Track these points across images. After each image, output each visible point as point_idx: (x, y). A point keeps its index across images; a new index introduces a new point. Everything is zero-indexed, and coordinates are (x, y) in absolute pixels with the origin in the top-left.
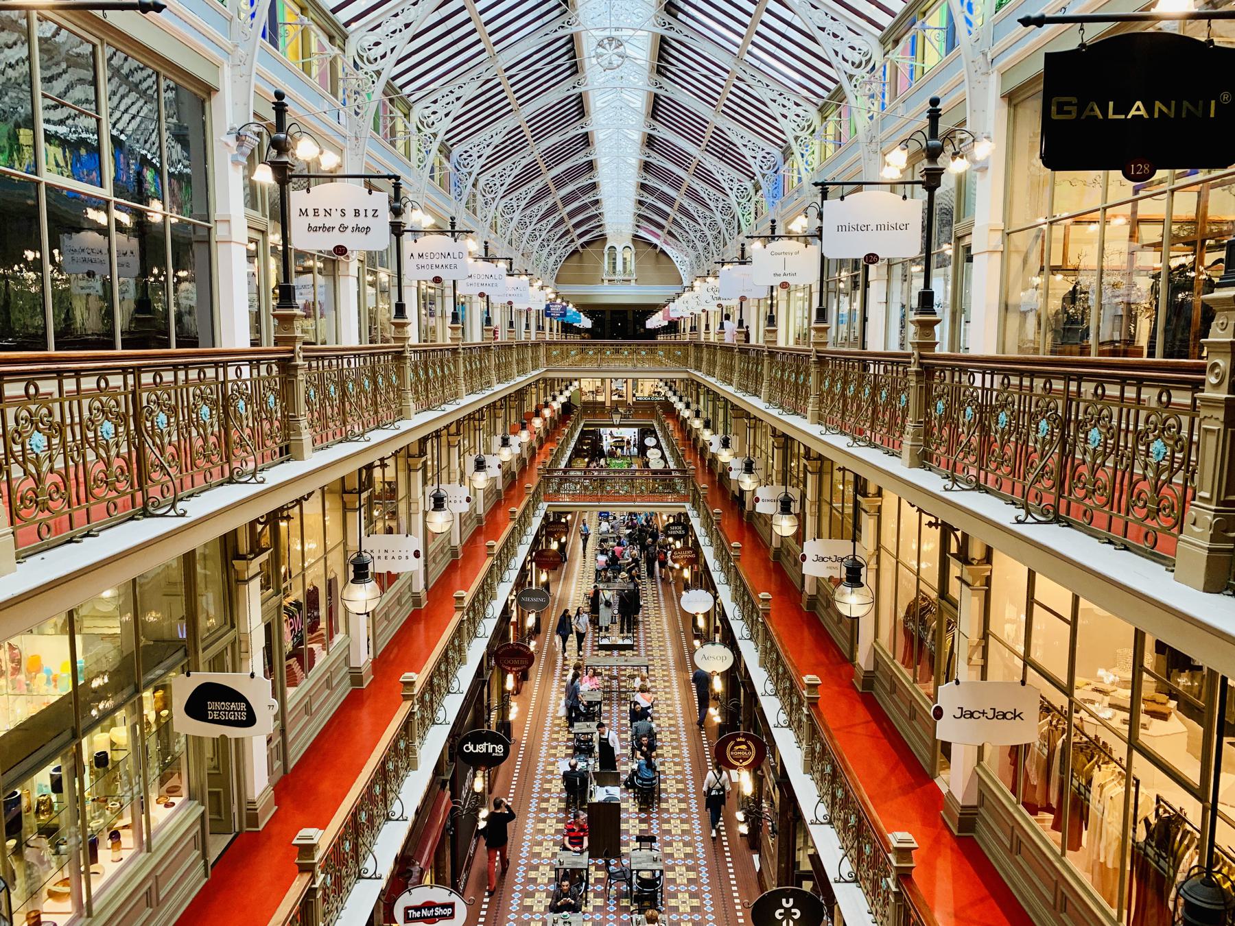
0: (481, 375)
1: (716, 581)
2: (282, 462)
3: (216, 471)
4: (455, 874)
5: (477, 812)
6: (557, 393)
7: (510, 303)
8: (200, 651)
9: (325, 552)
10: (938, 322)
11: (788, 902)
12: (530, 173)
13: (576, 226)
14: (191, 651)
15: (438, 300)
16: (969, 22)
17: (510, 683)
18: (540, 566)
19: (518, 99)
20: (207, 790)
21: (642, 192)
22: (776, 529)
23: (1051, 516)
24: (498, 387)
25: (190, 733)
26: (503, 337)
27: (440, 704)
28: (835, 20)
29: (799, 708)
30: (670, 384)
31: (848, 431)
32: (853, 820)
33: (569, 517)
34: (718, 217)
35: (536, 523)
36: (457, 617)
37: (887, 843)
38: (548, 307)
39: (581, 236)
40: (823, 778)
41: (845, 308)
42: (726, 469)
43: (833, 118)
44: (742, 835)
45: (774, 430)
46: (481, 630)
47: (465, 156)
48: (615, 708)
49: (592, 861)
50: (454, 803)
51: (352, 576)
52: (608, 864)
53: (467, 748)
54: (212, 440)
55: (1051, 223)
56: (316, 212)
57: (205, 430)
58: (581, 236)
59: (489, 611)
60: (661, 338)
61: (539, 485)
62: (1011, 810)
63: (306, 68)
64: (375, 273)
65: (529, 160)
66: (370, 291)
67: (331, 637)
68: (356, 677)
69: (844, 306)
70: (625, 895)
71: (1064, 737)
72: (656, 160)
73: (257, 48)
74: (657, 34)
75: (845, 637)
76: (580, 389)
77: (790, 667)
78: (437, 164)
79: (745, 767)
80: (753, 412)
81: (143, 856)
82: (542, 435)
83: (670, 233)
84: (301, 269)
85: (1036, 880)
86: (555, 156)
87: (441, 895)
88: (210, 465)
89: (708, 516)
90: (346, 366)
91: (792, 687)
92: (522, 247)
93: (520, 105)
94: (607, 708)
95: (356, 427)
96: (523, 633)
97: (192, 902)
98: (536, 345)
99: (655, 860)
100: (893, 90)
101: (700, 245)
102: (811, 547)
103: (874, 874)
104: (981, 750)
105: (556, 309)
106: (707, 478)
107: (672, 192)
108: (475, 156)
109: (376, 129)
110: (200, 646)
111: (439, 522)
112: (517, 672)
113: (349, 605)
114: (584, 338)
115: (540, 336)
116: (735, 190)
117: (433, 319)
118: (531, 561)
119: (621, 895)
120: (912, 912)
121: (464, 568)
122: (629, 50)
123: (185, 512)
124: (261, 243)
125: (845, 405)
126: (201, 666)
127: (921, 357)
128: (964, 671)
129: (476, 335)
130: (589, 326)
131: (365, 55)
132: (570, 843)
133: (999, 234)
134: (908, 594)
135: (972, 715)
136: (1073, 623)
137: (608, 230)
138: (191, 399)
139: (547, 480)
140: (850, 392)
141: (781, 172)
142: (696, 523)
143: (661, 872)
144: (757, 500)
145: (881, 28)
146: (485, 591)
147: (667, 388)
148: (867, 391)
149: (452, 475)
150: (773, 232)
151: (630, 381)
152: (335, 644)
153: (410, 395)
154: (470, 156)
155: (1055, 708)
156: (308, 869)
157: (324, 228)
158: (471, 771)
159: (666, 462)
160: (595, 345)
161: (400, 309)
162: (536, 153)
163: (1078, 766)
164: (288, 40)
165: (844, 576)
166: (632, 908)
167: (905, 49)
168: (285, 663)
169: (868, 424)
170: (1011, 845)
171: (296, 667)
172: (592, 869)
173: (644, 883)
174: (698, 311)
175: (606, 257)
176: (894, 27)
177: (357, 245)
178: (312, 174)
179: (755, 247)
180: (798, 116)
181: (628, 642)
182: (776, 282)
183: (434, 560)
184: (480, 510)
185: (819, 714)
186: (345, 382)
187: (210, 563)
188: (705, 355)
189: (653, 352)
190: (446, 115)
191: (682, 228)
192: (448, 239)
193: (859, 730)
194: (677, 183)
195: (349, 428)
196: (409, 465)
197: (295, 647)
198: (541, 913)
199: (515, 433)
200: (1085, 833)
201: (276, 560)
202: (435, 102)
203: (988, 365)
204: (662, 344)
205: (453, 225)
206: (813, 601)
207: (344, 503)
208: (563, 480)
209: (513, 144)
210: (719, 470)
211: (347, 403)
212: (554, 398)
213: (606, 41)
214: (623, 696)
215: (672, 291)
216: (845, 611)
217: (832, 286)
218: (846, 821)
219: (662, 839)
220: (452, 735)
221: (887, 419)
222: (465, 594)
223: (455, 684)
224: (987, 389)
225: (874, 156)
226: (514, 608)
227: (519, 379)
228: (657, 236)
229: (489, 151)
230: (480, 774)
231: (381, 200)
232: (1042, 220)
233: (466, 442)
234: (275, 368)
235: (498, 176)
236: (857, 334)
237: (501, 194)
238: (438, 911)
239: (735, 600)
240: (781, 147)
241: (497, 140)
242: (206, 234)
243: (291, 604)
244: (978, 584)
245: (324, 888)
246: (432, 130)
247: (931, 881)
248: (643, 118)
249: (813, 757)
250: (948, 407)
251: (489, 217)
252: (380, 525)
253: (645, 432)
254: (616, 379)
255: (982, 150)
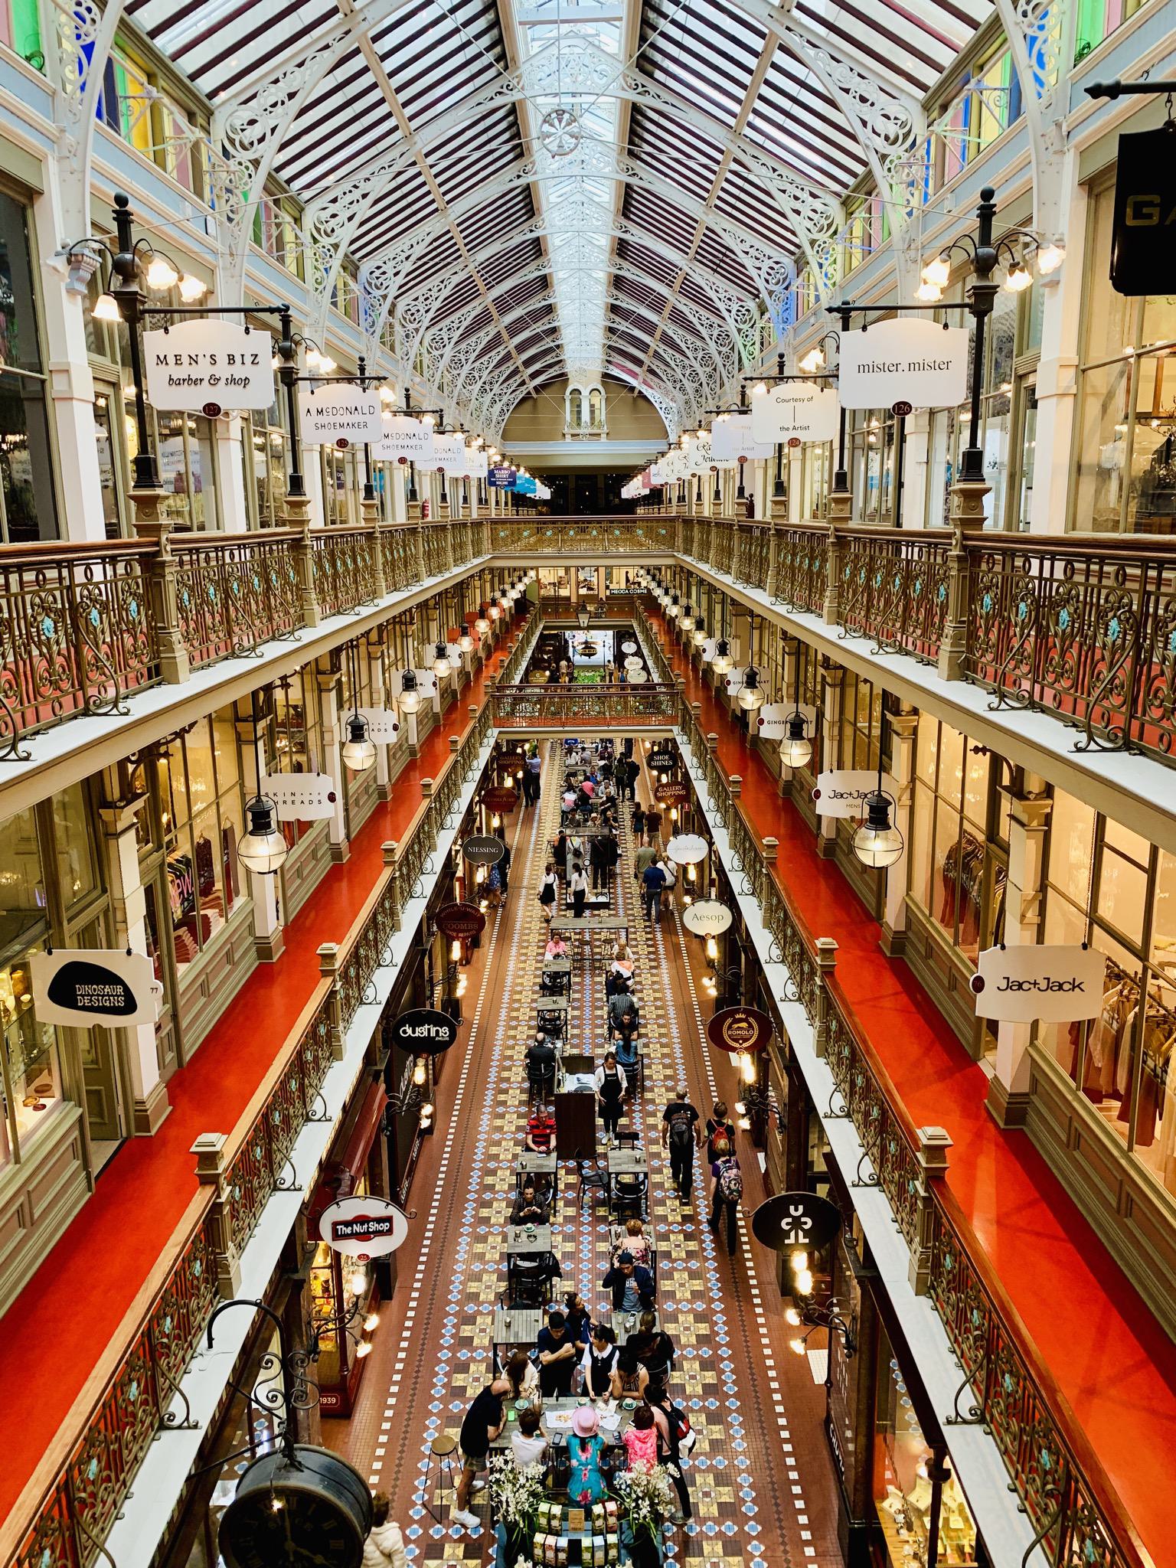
0: (406, 567)
1: (711, 823)
2: (152, 687)
3: (67, 701)
4: (395, 1183)
5: (420, 1108)
6: (507, 587)
7: (440, 470)
8: (65, 923)
9: (217, 797)
10: (988, 490)
11: (796, 1210)
12: (463, 294)
13: (527, 363)
14: (54, 923)
15: (348, 468)
16: (1037, 79)
17: (456, 952)
18: (492, 808)
19: (444, 194)
20: (84, 1088)
21: (613, 316)
22: (785, 759)
23: (1121, 742)
24: (428, 582)
25: (60, 1023)
26: (433, 516)
27: (369, 980)
28: (863, 78)
29: (811, 979)
30: (653, 572)
31: (873, 634)
32: (875, 1113)
33: (527, 746)
34: (712, 347)
35: (484, 754)
36: (386, 874)
37: (915, 1139)
38: (491, 473)
39: (533, 376)
40: (839, 1063)
41: (875, 471)
42: (724, 682)
43: (861, 214)
44: (744, 1131)
45: (784, 633)
46: (418, 889)
47: (377, 273)
48: (588, 980)
49: (561, 1163)
50: (391, 1097)
51: (250, 827)
52: (580, 1167)
53: (405, 1032)
54: (59, 660)
55: (1139, 356)
56: (178, 359)
57: (49, 649)
58: (533, 376)
59: (428, 865)
60: (640, 511)
61: (487, 706)
62: (1069, 1097)
63: (159, 159)
64: (264, 434)
65: (462, 276)
66: (259, 457)
67: (230, 900)
68: (263, 949)
69: (876, 465)
70: (602, 1203)
71: (1137, 1009)
72: (630, 272)
73: (91, 132)
74: (627, 101)
75: (871, 890)
76: (538, 581)
77: (800, 928)
78: (341, 286)
79: (746, 1049)
80: (757, 610)
81: (11, 1167)
82: (490, 641)
83: (652, 371)
84: (167, 432)
85: (1096, 1179)
86: (496, 270)
87: (376, 1208)
88: (59, 694)
89: (700, 742)
90: (228, 560)
91: (803, 952)
92: (456, 393)
93: (448, 202)
94: (577, 980)
95: (245, 638)
96: (471, 891)
97: (73, 1222)
98: (477, 525)
99: (638, 1161)
100: (939, 174)
101: (690, 387)
102: (825, 782)
103: (900, 1176)
104: (1035, 1025)
105: (502, 475)
106: (701, 694)
107: (652, 317)
108: (390, 273)
109: (257, 240)
110: (65, 916)
111: (359, 756)
112: (464, 939)
113: (247, 861)
114: (541, 514)
115: (484, 512)
116: (734, 312)
117: (342, 491)
118: (480, 802)
119: (597, 1203)
120: (944, 1220)
121: (394, 812)
122: (588, 122)
123: (29, 755)
124: (112, 398)
125: (870, 600)
126: (67, 941)
127: (965, 537)
128: (1015, 933)
129: (399, 514)
130: (548, 497)
131: (237, 138)
132: (534, 1142)
133: (1072, 371)
134: (949, 836)
135: (1020, 986)
136: (1151, 871)
137: (570, 368)
138: (28, 607)
139: (496, 700)
140: (877, 583)
141: (793, 288)
142: (686, 751)
143: (646, 1175)
144: (761, 722)
145: (923, 87)
146: (422, 842)
147: (649, 578)
148: (897, 582)
149: (375, 696)
150: (781, 371)
151: (602, 570)
152: (235, 909)
153: (313, 596)
154: (384, 273)
155: (1127, 975)
156: (212, 1180)
157: (189, 380)
158: (411, 1058)
159: (649, 673)
160: (554, 523)
161: (296, 484)
162: (471, 266)
163: (1155, 1044)
164: (132, 120)
165: (866, 816)
166: (611, 1218)
167: (955, 117)
168: (173, 935)
169: (898, 625)
170: (1069, 1140)
171: (188, 939)
172: (562, 1172)
173: (624, 1188)
174: (687, 477)
175: (568, 403)
176: (942, 85)
177: (233, 401)
178: (175, 307)
179: (758, 390)
180: (815, 211)
181: (602, 899)
182: (784, 438)
183: (357, 801)
184: (413, 740)
185: (835, 986)
186: (227, 581)
187: (70, 812)
188: (696, 534)
189: (629, 530)
190: (350, 219)
191: (667, 364)
192: (354, 389)
193: (887, 1003)
194: (657, 303)
195: (235, 640)
196: (319, 684)
197: (185, 913)
198: (500, 1225)
199: (453, 641)
200: (1158, 1124)
201: (155, 807)
202: (334, 201)
203: (1049, 548)
204: (642, 520)
205: (362, 369)
206: (831, 846)
207: (238, 735)
208: (517, 700)
209: (440, 254)
210: (716, 683)
211: (232, 609)
212: (504, 593)
213: (554, 115)
214: (597, 964)
215: (654, 447)
216: (866, 859)
217: (859, 440)
218: (867, 1114)
219: (646, 1135)
220: (385, 1016)
221: (921, 618)
222: (395, 845)
223: (387, 955)
224: (1046, 580)
225: (913, 266)
226: (459, 860)
227: (456, 570)
228: (634, 375)
229: (408, 266)
230: (421, 1062)
231: (262, 341)
232: (1129, 351)
233: (392, 652)
234: (138, 570)
235: (421, 299)
236: (890, 504)
237: (426, 323)
238: (373, 1226)
239: (733, 846)
240: (792, 253)
241: (420, 251)
242: (38, 387)
243: (177, 861)
244: (1035, 823)
245: (232, 1202)
246: (332, 240)
247: (970, 1181)
248: (611, 216)
249: (828, 1037)
250: (999, 601)
251: (412, 356)
252: (285, 761)
253: (623, 635)
254: (583, 568)
255: (1048, 260)
